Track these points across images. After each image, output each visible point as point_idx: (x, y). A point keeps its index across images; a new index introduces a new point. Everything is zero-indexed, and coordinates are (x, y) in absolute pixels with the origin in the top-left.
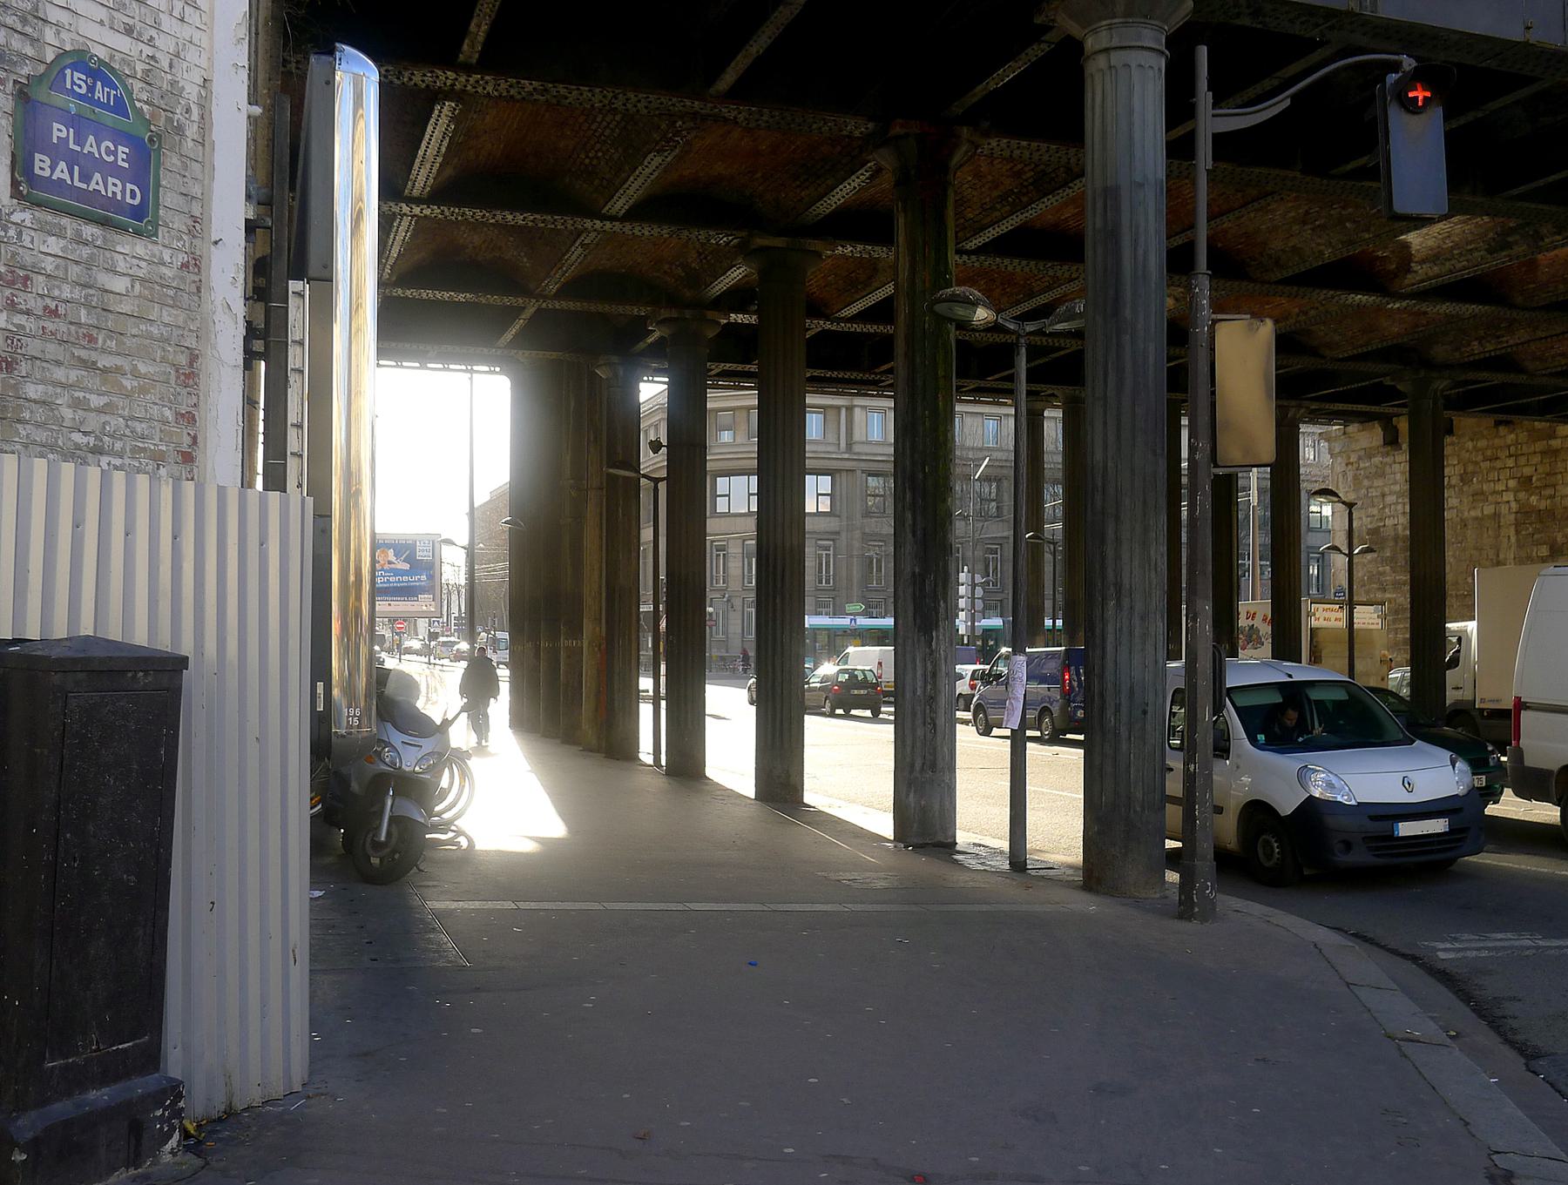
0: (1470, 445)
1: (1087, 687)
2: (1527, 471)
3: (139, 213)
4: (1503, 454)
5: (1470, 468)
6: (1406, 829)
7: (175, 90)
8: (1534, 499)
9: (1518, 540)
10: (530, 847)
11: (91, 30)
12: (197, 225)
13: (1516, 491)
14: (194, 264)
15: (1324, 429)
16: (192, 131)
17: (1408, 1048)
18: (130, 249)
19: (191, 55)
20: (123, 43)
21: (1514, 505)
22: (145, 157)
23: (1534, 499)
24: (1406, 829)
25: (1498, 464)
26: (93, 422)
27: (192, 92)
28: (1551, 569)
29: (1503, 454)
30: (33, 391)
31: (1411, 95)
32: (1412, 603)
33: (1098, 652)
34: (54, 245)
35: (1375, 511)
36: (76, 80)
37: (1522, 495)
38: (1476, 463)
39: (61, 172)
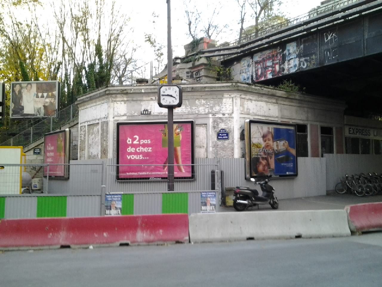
1: (142, 93)
3: (228, 138)
6: (312, 30)
7: (230, 128)
11: (223, 127)
12: (233, 138)
14: (233, 141)
15: (298, 21)
16: (232, 131)
18: (227, 142)
19: (232, 125)
20: (226, 126)
22: (227, 135)
24: (312, 30)
26: (224, 154)
27: (232, 128)
28: (5, 217)
30: (219, 153)
31: (134, 137)
34: (220, 143)
36: (222, 131)
39: (221, 137)
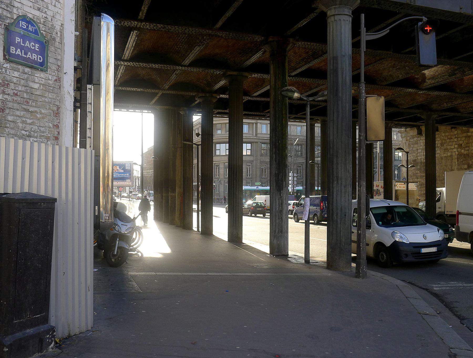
0: (443, 134)
1: (328, 208)
2: (461, 142)
3: (42, 64)
4: (453, 137)
5: (444, 141)
6: (424, 250)
7: (53, 27)
8: (463, 151)
9: (458, 163)
10: (160, 256)
11: (27, 9)
12: (59, 68)
13: (457, 148)
14: (59, 80)
15: (400, 129)
16: (58, 40)
17: (425, 317)
18: (39, 75)
19: (58, 17)
20: (37, 13)
21: (457, 153)
22: (44, 47)
23: (463, 151)
24: (424, 250)
25: (452, 140)
26: (28, 127)
27: (58, 28)
28: (468, 172)
29: (453, 137)
30: (10, 118)
31: (426, 29)
32: (426, 182)
33: (331, 197)
34: (16, 74)
35: (415, 154)
36: (23, 24)
37: (459, 150)
38: (445, 140)
39: (19, 52)
